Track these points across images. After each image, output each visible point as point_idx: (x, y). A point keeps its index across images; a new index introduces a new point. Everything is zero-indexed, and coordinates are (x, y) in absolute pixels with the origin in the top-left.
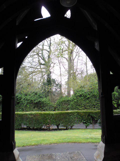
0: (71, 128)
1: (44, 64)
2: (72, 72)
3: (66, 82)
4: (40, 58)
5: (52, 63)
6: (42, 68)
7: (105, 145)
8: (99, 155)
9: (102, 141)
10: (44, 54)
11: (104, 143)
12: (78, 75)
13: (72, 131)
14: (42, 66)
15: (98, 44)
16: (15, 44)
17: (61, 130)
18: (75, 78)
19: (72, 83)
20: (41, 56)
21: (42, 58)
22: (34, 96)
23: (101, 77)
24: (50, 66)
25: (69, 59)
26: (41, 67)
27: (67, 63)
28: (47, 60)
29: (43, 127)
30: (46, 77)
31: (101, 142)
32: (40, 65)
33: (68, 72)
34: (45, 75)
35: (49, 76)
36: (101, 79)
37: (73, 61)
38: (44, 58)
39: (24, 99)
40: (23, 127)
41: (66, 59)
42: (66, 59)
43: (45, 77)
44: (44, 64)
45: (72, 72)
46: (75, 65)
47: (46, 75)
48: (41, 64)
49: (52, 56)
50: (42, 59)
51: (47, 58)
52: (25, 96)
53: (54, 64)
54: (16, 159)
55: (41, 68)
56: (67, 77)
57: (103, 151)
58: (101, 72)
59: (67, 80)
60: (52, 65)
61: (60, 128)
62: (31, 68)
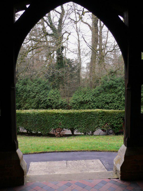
0: (92, 134)
1: (50, 35)
2: (98, 48)
3: (88, 63)
4: (45, 23)
5: (66, 32)
6: (48, 40)
7: (127, 149)
8: (119, 160)
9: (124, 144)
10: (52, 18)
11: (125, 146)
12: (108, 53)
13: (92, 137)
14: (49, 38)
15: (128, 16)
16: (13, 19)
17: (75, 135)
18: (102, 57)
19: (97, 66)
20: (47, 21)
21: (49, 24)
22: (36, 86)
23: (128, 63)
24: (62, 38)
25: (94, 27)
26: (46, 40)
27: (90, 32)
28: (56, 27)
29: (51, 132)
30: (56, 56)
31: (123, 145)
32: (46, 35)
33: (91, 47)
34: (53, 51)
35: (59, 53)
36: (128, 65)
37: (101, 30)
38: (51, 23)
39: (21, 90)
40: (21, 131)
41: (89, 25)
42: (89, 25)
43: (54, 55)
44: (50, 35)
45: (98, 48)
46: (104, 36)
47: (55, 52)
48: (47, 34)
49: (66, 21)
50: (48, 25)
51: (58, 23)
52: (23, 85)
53: (68, 34)
54: (20, 159)
55: (46, 41)
56: (89, 57)
57: (124, 155)
58: (128, 56)
59: (89, 61)
60: (65, 36)
61: (75, 133)
62: (31, 41)
